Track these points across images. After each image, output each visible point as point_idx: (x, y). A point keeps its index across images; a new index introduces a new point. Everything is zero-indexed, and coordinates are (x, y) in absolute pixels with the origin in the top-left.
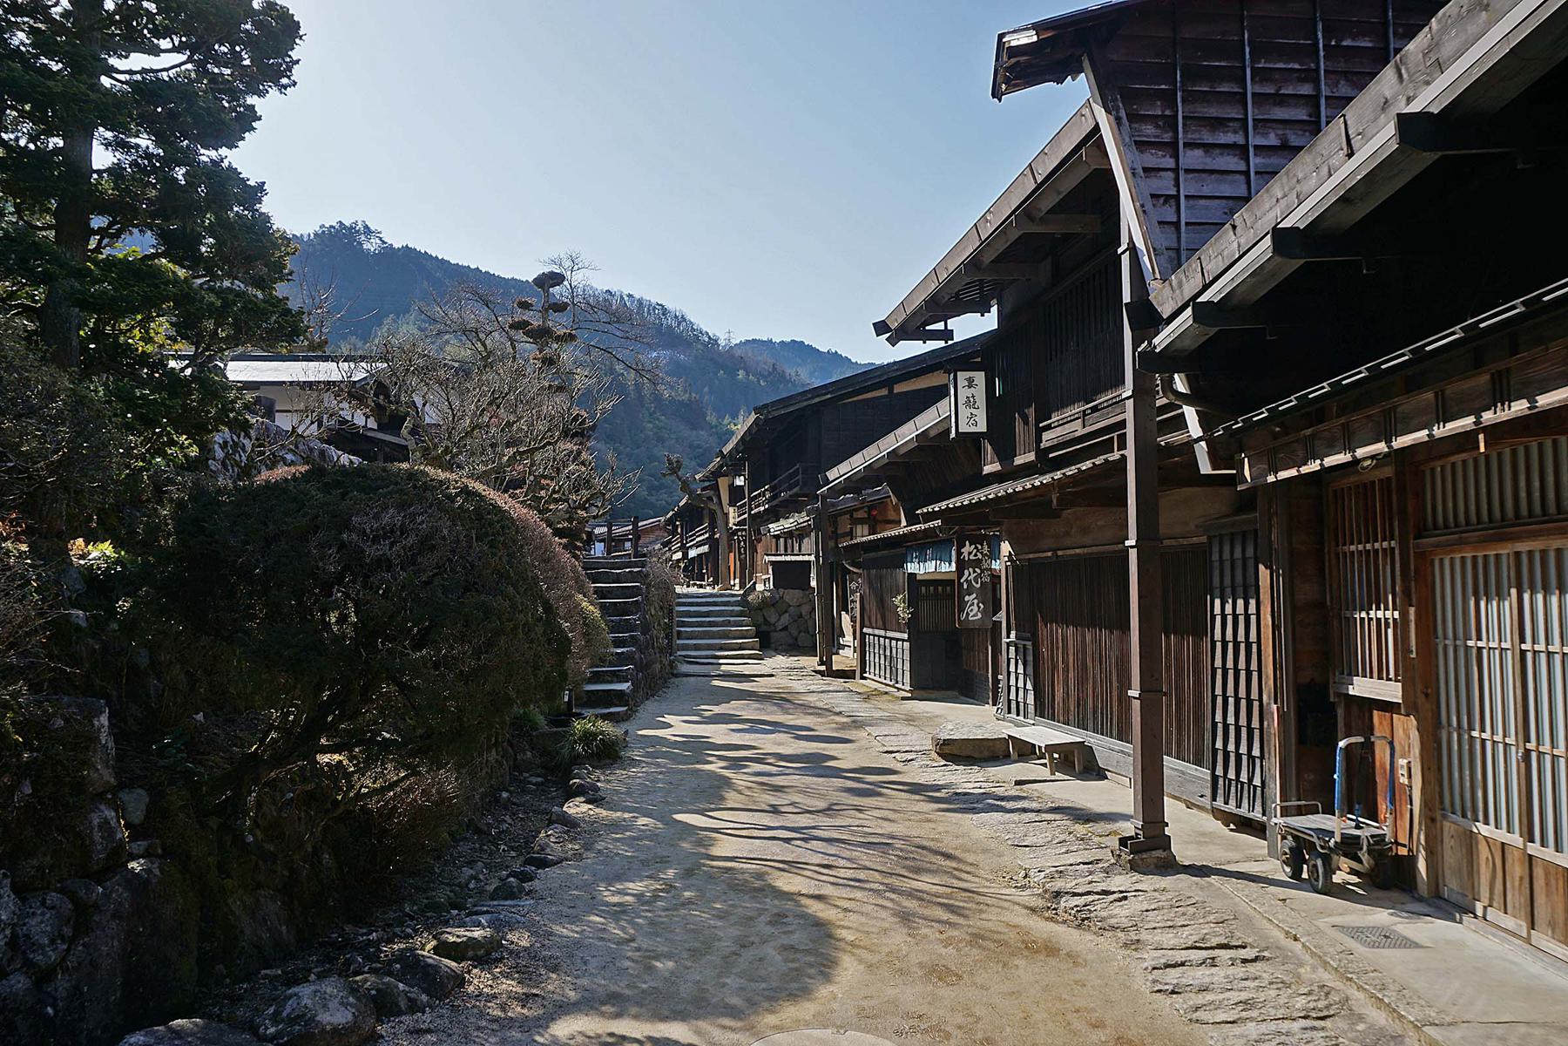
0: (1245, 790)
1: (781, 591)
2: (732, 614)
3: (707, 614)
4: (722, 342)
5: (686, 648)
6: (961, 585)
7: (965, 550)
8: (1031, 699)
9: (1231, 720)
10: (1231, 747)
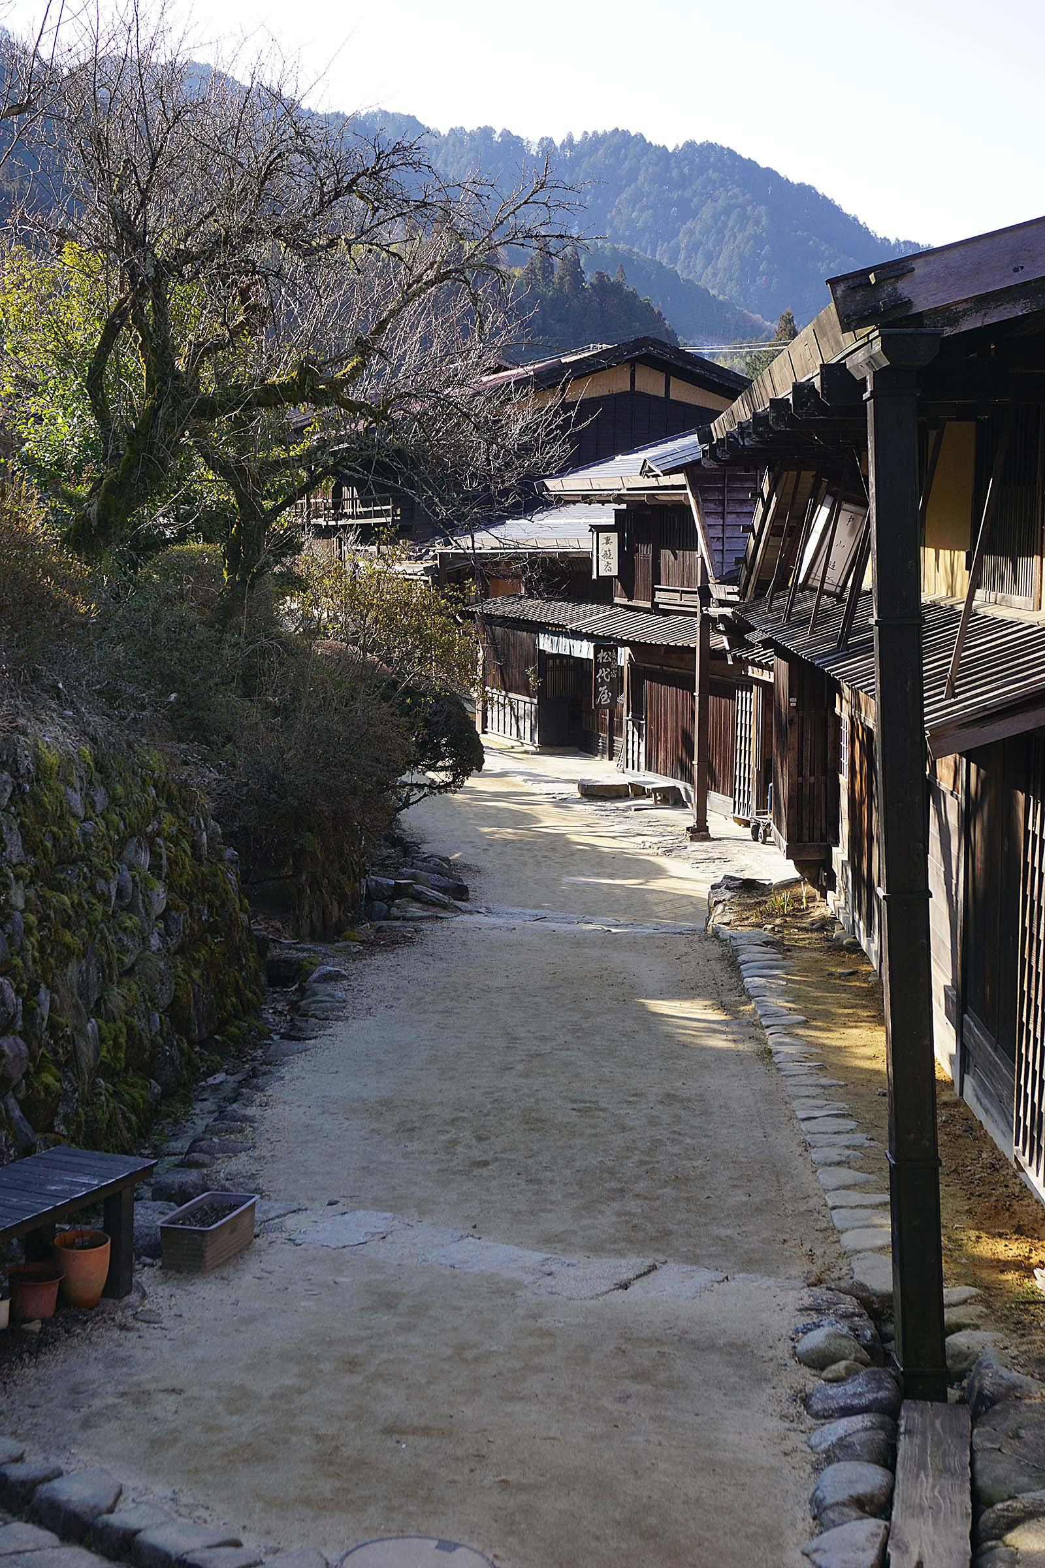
6: (596, 680)
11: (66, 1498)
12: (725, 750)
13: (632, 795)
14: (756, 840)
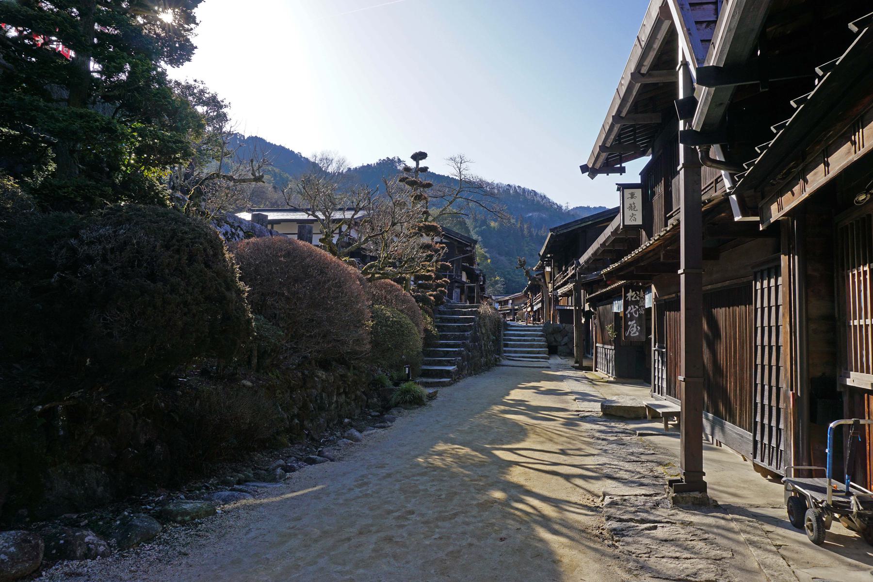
0: (777, 454)
1: (564, 325)
2: (537, 336)
3: (524, 336)
4: (564, 208)
5: (510, 352)
7: (629, 295)
8: (665, 385)
9: (766, 402)
10: (766, 421)
11: (562, 570)
12: (742, 369)
13: (649, 417)
14: (798, 524)
